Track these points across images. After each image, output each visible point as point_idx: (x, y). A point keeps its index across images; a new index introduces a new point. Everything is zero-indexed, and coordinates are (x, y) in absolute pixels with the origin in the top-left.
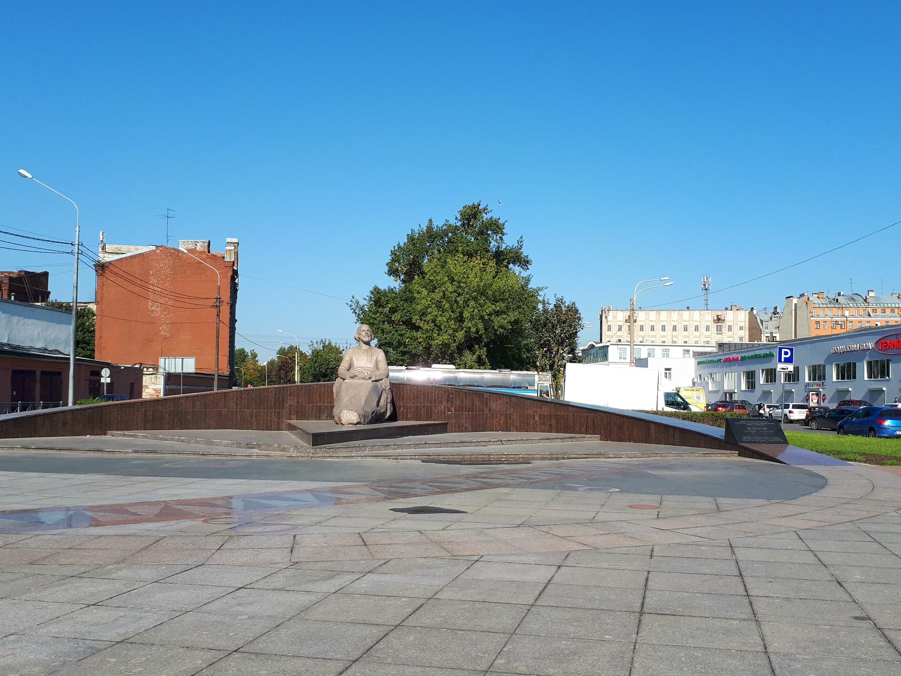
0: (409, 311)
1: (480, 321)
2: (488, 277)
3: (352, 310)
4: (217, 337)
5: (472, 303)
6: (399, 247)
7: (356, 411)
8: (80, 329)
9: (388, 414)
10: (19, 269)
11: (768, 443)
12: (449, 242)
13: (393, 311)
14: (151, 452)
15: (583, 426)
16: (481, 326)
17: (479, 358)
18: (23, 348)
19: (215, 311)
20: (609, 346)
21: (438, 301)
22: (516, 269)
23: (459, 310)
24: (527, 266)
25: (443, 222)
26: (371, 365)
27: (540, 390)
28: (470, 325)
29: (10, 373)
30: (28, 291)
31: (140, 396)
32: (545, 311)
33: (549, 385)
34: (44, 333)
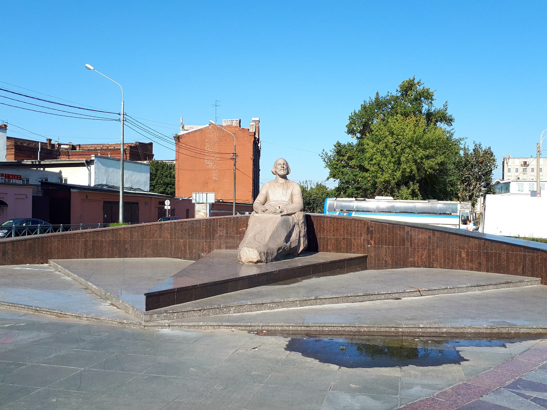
0: (362, 159)
1: (414, 164)
5: (407, 150)
6: (355, 114)
7: (257, 249)
9: (301, 248)
10: (135, 141)
12: (392, 108)
13: (350, 158)
15: (520, 266)
16: (414, 167)
19: (233, 162)
20: (510, 182)
21: (382, 150)
22: (442, 125)
23: (397, 156)
24: (451, 123)
25: (386, 94)
26: (286, 199)
28: (405, 166)
29: (102, 204)
30: (141, 154)
31: (193, 217)
32: (466, 154)
33: (469, 212)
34: (130, 178)
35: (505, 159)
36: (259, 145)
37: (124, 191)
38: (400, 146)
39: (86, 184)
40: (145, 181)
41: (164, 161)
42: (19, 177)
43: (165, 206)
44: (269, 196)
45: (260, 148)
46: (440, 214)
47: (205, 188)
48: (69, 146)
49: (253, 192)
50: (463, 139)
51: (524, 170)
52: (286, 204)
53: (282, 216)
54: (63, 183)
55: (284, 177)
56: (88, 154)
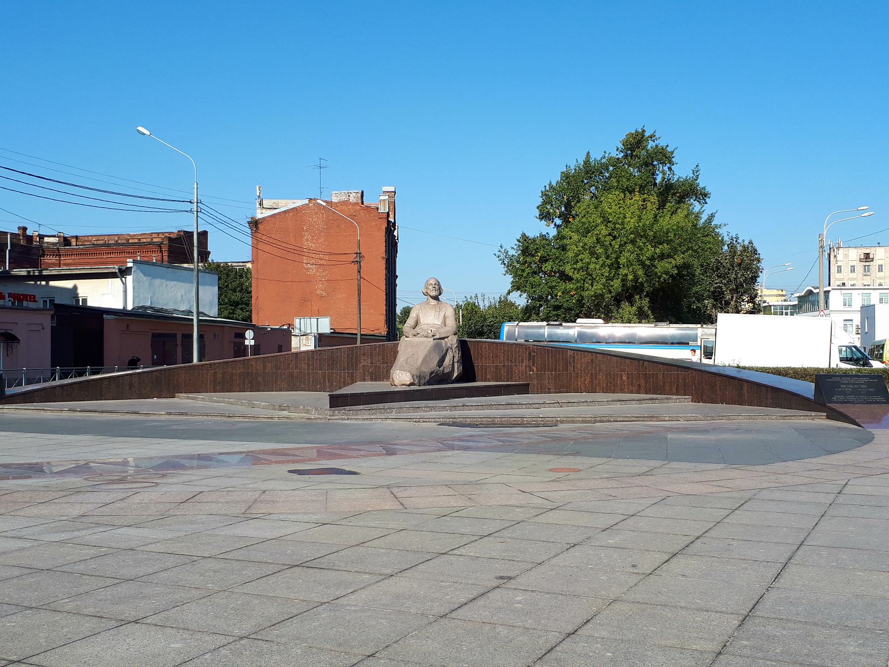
1: (640, 267)
2: (648, 218)
3: (501, 261)
4: (358, 295)
5: (629, 247)
6: (551, 187)
7: (409, 371)
8: (239, 289)
9: (455, 375)
11: (865, 404)
13: (544, 260)
14: (182, 414)
16: (640, 272)
17: (640, 309)
18: (166, 310)
19: (356, 266)
20: (830, 291)
24: (704, 200)
26: (439, 322)
27: (704, 346)
28: (626, 271)
29: (148, 339)
30: (188, 251)
35: (832, 250)
36: (395, 233)
37: (200, 318)
38: (619, 240)
39: (120, 306)
40: (210, 300)
41: (230, 264)
42: (32, 298)
43: (246, 340)
44: (420, 319)
45: (396, 238)
46: (672, 343)
47: (307, 310)
48: (57, 239)
49: (386, 315)
50: (720, 225)
51: (865, 270)
52: (438, 327)
53: (434, 339)
54: (81, 304)
55: (436, 298)
56: (94, 254)
